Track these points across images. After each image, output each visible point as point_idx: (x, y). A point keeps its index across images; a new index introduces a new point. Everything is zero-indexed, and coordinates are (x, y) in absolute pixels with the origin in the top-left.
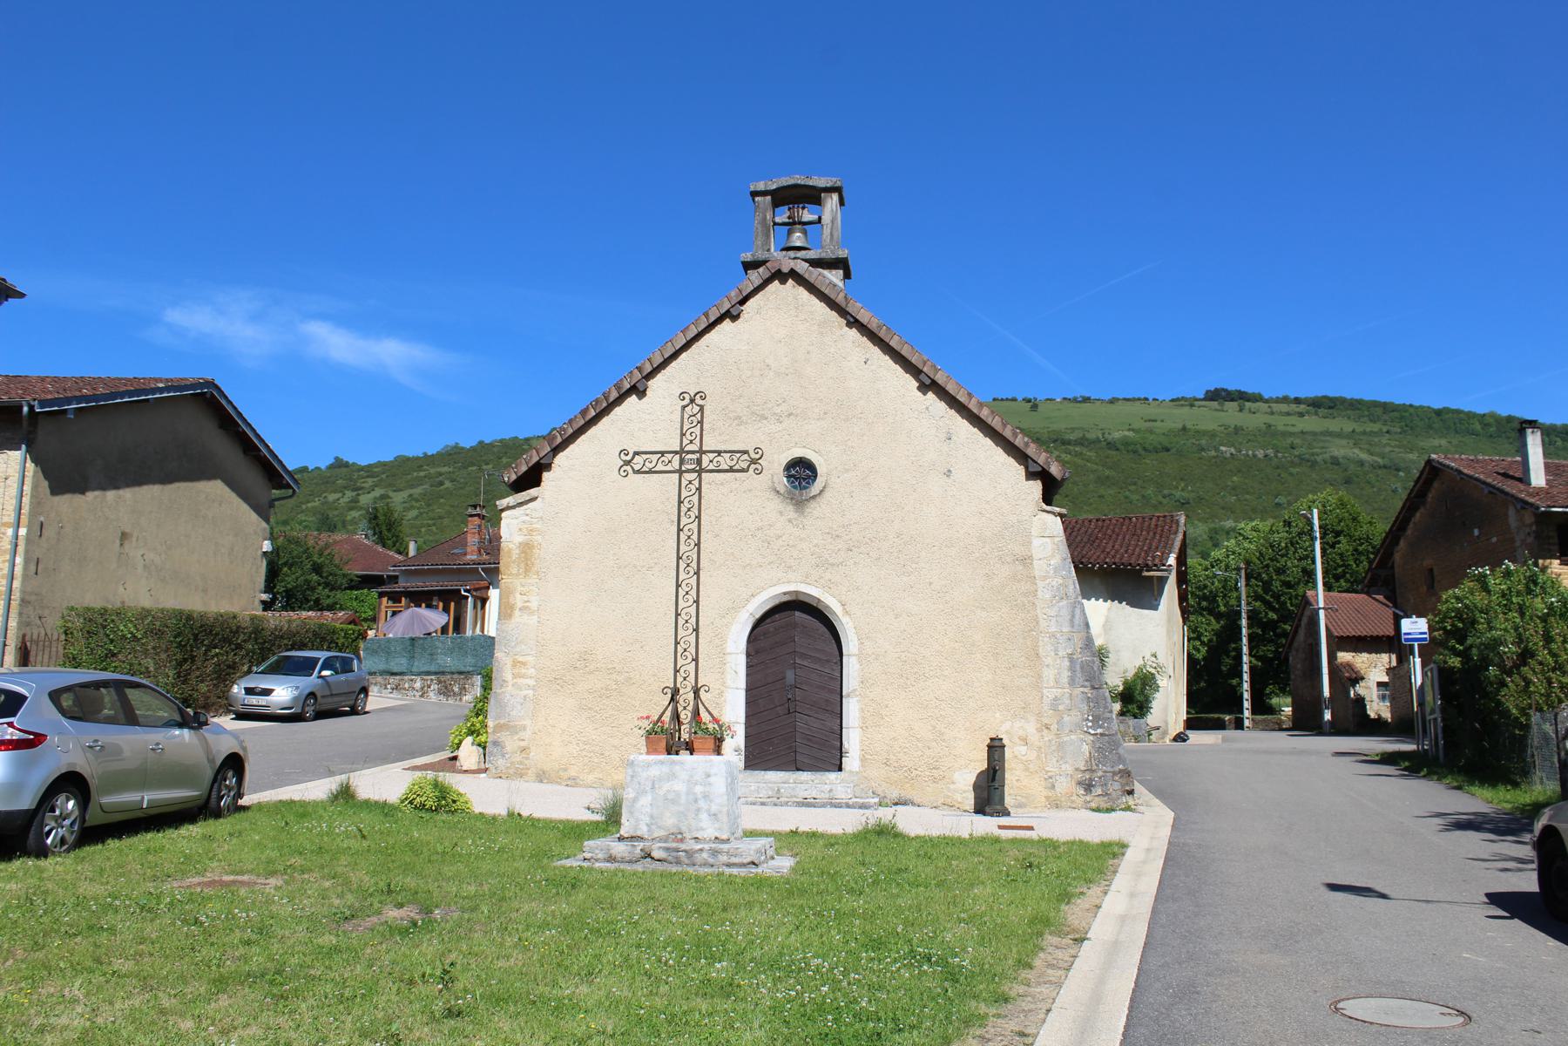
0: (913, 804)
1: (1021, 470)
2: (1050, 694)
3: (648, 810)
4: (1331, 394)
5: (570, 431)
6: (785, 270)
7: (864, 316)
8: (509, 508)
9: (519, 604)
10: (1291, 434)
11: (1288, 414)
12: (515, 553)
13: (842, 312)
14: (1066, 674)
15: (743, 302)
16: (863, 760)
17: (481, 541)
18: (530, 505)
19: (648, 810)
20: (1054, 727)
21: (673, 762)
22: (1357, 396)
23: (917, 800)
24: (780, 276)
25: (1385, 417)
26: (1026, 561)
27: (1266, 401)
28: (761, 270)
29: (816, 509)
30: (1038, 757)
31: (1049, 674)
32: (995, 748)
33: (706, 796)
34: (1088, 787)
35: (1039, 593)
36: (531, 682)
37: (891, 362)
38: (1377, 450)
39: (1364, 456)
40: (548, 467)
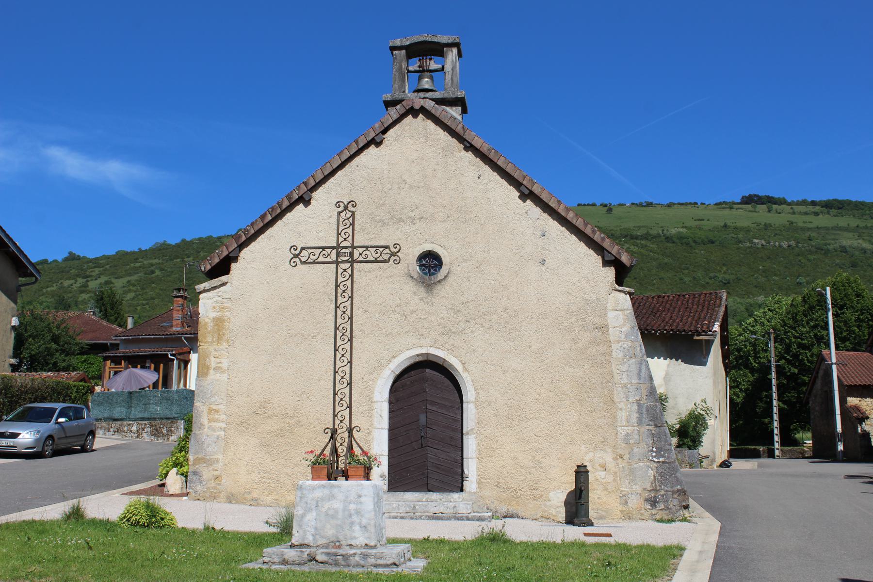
0: (518, 517)
1: (599, 259)
2: (623, 431)
3: (313, 523)
4: (840, 198)
5: (252, 232)
6: (417, 107)
7: (477, 142)
8: (205, 291)
9: (213, 365)
10: (809, 229)
11: (806, 214)
12: (210, 326)
13: (461, 139)
14: (635, 416)
15: (384, 132)
16: (479, 483)
17: (184, 317)
19: (313, 523)
20: (626, 457)
21: (332, 486)
23: (521, 514)
24: (413, 112)
26: (603, 328)
28: (398, 107)
29: (442, 290)
30: (614, 480)
31: (622, 416)
33: (358, 512)
34: (653, 503)
35: (614, 354)
36: (223, 425)
37: (498, 177)
40: (235, 259)
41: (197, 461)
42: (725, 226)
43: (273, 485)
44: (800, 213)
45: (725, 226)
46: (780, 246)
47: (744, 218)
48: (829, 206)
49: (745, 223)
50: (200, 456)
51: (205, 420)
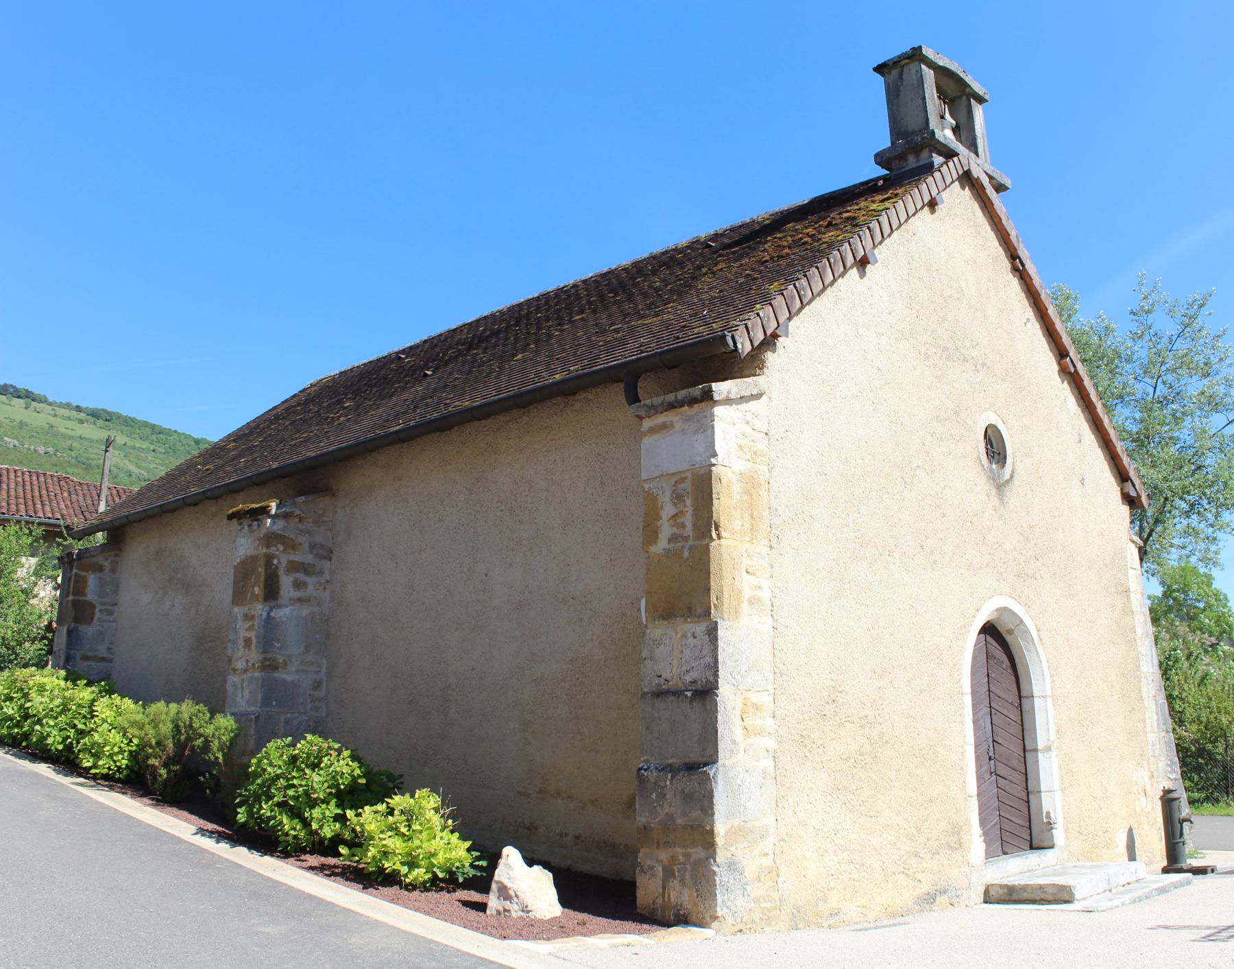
4: (109, 409)
8: (728, 401)
9: (747, 593)
10: (71, 437)
11: (69, 419)
13: (1013, 256)
18: (753, 405)
22: (132, 415)
25: (154, 437)
26: (1127, 591)
27: (50, 404)
32: (1130, 831)
36: (771, 743)
38: (144, 464)
39: (133, 468)
41: (733, 833)
43: (856, 876)
44: (63, 417)
46: (35, 451)
48: (95, 414)
50: (736, 822)
51: (738, 733)
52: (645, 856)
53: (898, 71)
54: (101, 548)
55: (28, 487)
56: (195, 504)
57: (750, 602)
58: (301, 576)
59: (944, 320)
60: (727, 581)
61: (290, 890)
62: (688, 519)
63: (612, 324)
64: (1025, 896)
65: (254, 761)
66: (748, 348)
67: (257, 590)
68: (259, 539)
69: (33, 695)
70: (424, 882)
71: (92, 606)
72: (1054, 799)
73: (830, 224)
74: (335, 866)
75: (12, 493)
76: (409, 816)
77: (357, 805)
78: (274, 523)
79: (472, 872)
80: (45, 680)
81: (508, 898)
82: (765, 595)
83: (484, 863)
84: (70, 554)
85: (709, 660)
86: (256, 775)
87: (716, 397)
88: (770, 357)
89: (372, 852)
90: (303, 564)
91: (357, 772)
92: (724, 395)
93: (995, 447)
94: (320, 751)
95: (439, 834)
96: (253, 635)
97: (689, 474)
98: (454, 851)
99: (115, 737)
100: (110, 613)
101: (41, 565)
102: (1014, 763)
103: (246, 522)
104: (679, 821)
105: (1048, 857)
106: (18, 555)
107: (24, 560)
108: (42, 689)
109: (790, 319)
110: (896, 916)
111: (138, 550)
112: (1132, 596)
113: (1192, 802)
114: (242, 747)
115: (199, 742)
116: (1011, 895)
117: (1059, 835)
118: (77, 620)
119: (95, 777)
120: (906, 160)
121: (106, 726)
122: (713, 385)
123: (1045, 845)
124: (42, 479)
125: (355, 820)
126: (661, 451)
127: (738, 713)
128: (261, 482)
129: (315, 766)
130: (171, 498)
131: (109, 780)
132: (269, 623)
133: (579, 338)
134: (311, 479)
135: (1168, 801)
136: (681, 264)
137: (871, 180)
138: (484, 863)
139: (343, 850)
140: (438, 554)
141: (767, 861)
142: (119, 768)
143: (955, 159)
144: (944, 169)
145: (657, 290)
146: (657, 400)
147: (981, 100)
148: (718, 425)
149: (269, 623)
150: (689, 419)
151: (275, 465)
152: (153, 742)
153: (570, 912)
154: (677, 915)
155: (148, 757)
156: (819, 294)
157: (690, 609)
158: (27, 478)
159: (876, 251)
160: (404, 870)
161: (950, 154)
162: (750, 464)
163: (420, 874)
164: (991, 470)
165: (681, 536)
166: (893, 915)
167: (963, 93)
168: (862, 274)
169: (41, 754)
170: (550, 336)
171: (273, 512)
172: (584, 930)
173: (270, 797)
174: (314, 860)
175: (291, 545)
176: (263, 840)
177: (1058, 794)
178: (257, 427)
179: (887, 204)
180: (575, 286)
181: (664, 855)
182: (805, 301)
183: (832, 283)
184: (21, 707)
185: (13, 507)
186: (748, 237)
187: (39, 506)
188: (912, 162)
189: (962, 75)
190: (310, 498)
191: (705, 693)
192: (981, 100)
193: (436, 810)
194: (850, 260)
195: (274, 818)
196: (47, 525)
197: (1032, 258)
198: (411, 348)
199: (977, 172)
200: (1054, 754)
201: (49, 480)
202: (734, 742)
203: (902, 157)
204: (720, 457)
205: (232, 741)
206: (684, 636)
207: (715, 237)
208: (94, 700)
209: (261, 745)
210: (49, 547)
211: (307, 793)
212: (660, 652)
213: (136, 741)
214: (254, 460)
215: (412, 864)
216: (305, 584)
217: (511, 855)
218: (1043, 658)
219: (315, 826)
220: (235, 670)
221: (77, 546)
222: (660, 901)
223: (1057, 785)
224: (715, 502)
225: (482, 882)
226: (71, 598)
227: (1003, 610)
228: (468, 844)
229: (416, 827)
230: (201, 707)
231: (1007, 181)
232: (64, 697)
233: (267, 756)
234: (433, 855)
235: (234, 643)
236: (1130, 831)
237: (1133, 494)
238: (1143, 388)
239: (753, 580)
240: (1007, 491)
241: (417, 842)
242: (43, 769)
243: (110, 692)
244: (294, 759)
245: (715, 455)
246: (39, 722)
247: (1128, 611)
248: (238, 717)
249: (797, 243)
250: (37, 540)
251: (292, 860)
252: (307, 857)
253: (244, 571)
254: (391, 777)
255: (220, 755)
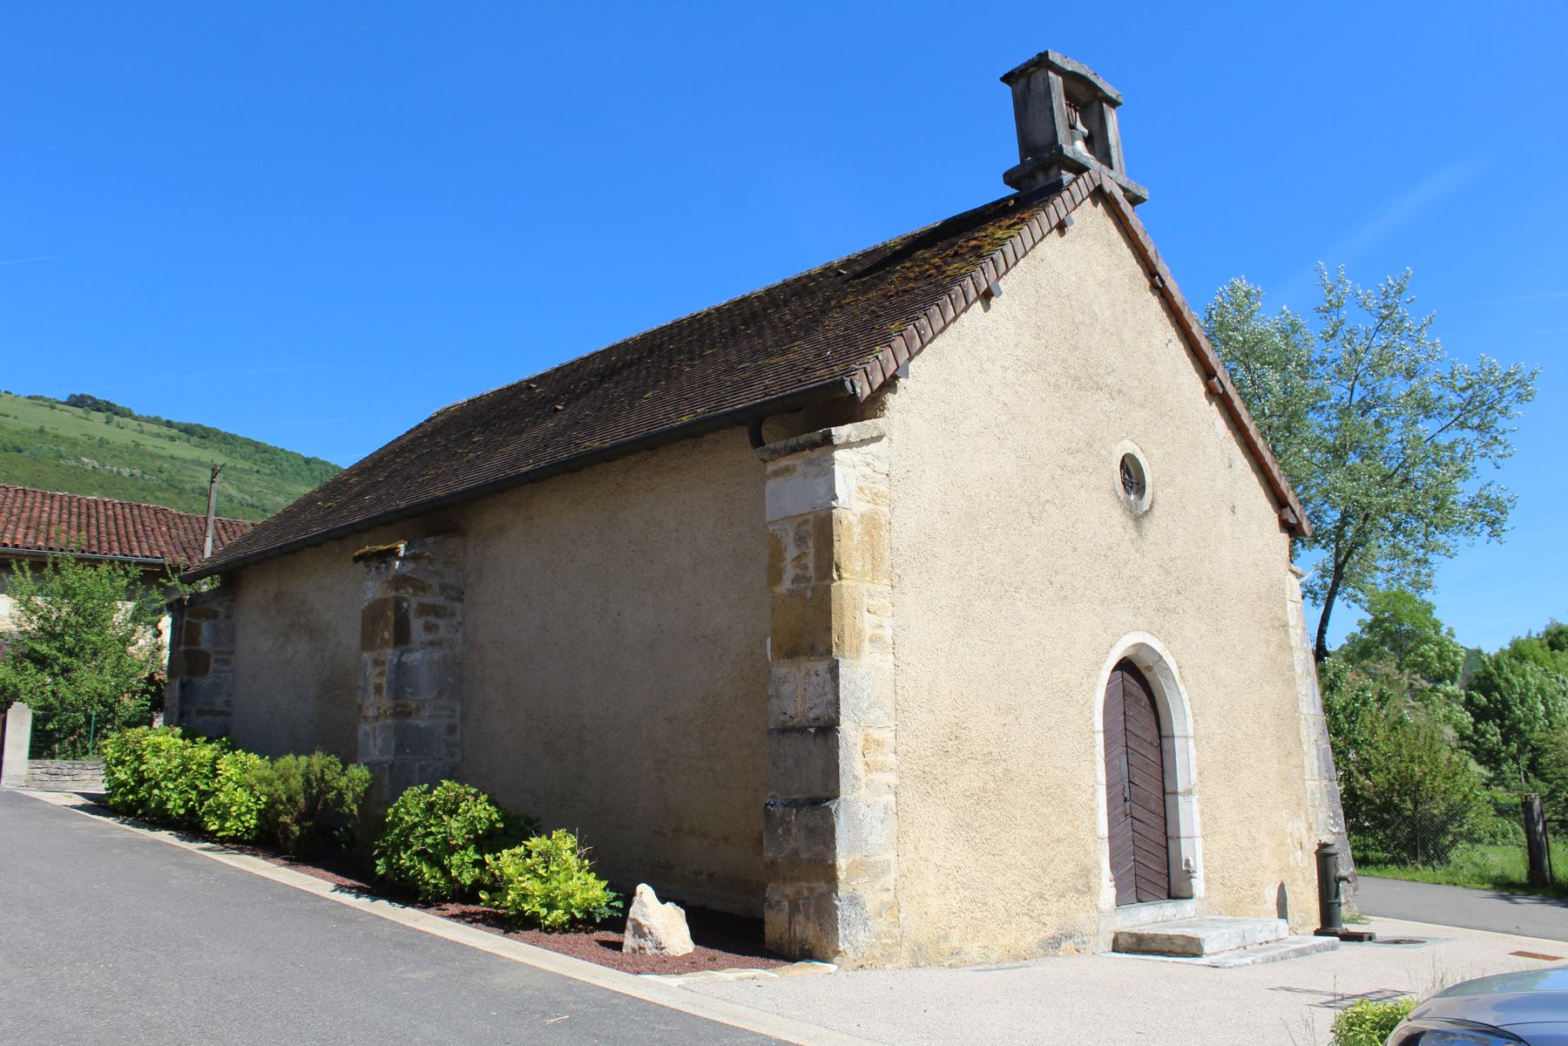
8: (848, 445)
9: (868, 632)
10: (160, 457)
11: (158, 435)
13: (1151, 272)
18: (873, 447)
26: (1285, 626)
32: (1282, 887)
36: (892, 779)
41: (856, 867)
42: (42, 431)
43: (979, 915)
45: (42, 431)
47: (71, 424)
48: (189, 430)
49: (71, 432)
51: (859, 768)
52: (773, 892)
53: (1026, 79)
54: (217, 594)
55: (121, 522)
56: (318, 545)
57: (871, 641)
58: (432, 619)
59: (1076, 348)
60: (848, 621)
61: (433, 938)
62: (810, 562)
63: (741, 362)
64: (1154, 946)
65: (391, 810)
66: (867, 391)
67: (386, 634)
68: (389, 582)
69: (148, 756)
70: (563, 924)
71: (206, 656)
72: (1196, 846)
73: (956, 254)
74: (476, 913)
75: (103, 529)
76: (547, 857)
77: (495, 849)
78: (402, 565)
79: (607, 913)
80: (161, 739)
81: (642, 935)
82: (887, 633)
83: (619, 904)
84: (180, 600)
85: (830, 697)
86: (393, 825)
87: (836, 441)
88: (891, 399)
89: (512, 895)
90: (434, 606)
91: (495, 816)
92: (844, 439)
93: (1132, 476)
94: (457, 797)
95: (576, 875)
96: (383, 681)
97: (811, 517)
98: (591, 890)
99: (242, 796)
100: (227, 662)
101: (139, 609)
102: (1153, 806)
103: (373, 565)
104: (804, 856)
105: (1187, 907)
106: (112, 599)
107: (119, 604)
108: (157, 750)
109: (910, 359)
110: (1019, 958)
111: (255, 595)
112: (1291, 631)
113: (1361, 862)
114: (378, 796)
115: (332, 795)
116: (1138, 945)
117: (1198, 885)
118: (190, 672)
119: (222, 841)
120: (1035, 178)
121: (231, 784)
122: (833, 429)
123: (1184, 894)
124: (136, 512)
125: (494, 864)
126: (784, 495)
127: (859, 749)
128: (389, 523)
129: (452, 812)
130: (291, 538)
131: (238, 843)
132: (401, 669)
133: (707, 376)
134: (441, 520)
135: (1324, 856)
136: (812, 293)
137: (1002, 200)
138: (619, 904)
139: (484, 896)
140: (573, 598)
141: (888, 897)
142: (248, 828)
143: (1086, 175)
144: (1074, 187)
145: (787, 323)
146: (780, 444)
147: (1114, 104)
148: (839, 470)
149: (401, 669)
150: (810, 463)
151: (403, 505)
152: (284, 798)
153: (702, 949)
154: (802, 950)
155: (278, 814)
156: (941, 332)
157: (812, 648)
158: (119, 511)
159: (1001, 283)
160: (543, 912)
161: (1079, 169)
162: (871, 506)
163: (559, 915)
164: (1128, 502)
165: (804, 577)
166: (1016, 958)
167: (1095, 97)
168: (987, 307)
169: (158, 819)
170: (681, 372)
171: (402, 553)
172: (714, 965)
173: (408, 846)
174: (454, 908)
175: (421, 587)
176: (405, 891)
177: (1199, 843)
178: (381, 460)
179: (1012, 232)
180: (708, 314)
181: (789, 890)
182: (926, 340)
183: (954, 320)
184: (135, 770)
185: (105, 545)
186: (877, 266)
187: (135, 543)
188: (1041, 181)
189: (1092, 78)
190: (439, 538)
191: (827, 729)
192: (1114, 104)
193: (573, 851)
194: (972, 294)
195: (413, 867)
196: (145, 564)
197: (1173, 274)
198: (542, 376)
199: (1110, 186)
200: (1195, 798)
201: (136, 512)
202: (855, 777)
203: (1031, 176)
204: (840, 500)
205: (367, 791)
206: (808, 674)
207: (848, 263)
208: (215, 759)
209: (397, 792)
210: (147, 590)
211: (445, 840)
212: (786, 689)
213: (264, 799)
214: (379, 498)
215: (551, 906)
216: (436, 627)
217: (645, 892)
218: (1185, 696)
219: (454, 873)
220: (366, 718)
221: (186, 591)
222: (786, 936)
223: (1198, 831)
224: (836, 544)
225: (617, 923)
226: (182, 648)
227: (1142, 646)
228: (604, 884)
229: (554, 868)
230: (333, 758)
231: (1144, 193)
232: (183, 757)
233: (404, 805)
234: (572, 895)
235: (365, 690)
236: (1282, 887)
237: (1292, 520)
238: (1338, 391)
239: (874, 619)
240: (1146, 523)
241: (555, 883)
242: (164, 836)
243: (233, 748)
244: (431, 806)
245: (835, 498)
246: (157, 785)
247: (1286, 648)
248: (372, 766)
249: (923, 275)
250: (133, 583)
251: (433, 910)
252: (448, 905)
253: (372, 616)
254: (529, 822)
255: (354, 807)
